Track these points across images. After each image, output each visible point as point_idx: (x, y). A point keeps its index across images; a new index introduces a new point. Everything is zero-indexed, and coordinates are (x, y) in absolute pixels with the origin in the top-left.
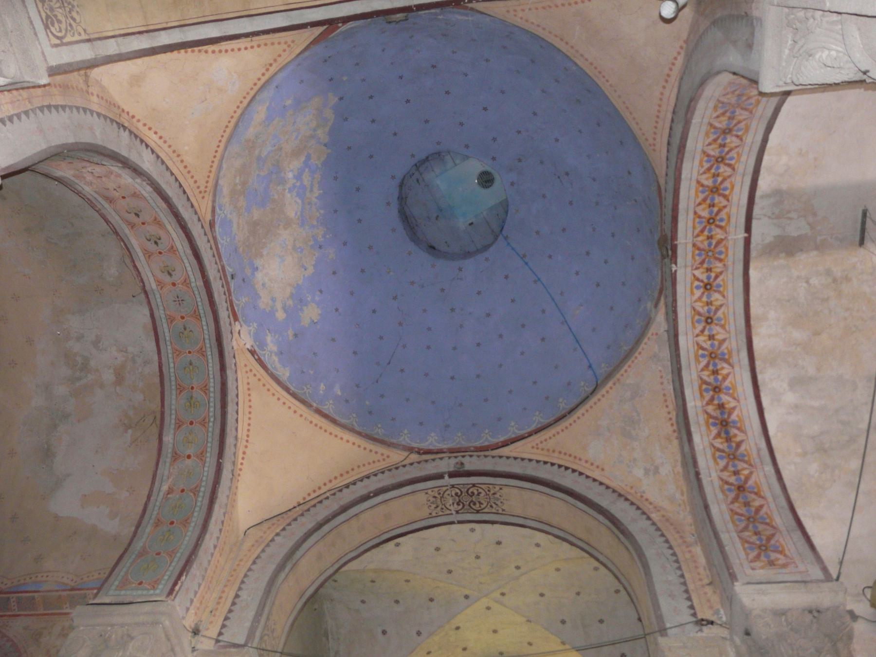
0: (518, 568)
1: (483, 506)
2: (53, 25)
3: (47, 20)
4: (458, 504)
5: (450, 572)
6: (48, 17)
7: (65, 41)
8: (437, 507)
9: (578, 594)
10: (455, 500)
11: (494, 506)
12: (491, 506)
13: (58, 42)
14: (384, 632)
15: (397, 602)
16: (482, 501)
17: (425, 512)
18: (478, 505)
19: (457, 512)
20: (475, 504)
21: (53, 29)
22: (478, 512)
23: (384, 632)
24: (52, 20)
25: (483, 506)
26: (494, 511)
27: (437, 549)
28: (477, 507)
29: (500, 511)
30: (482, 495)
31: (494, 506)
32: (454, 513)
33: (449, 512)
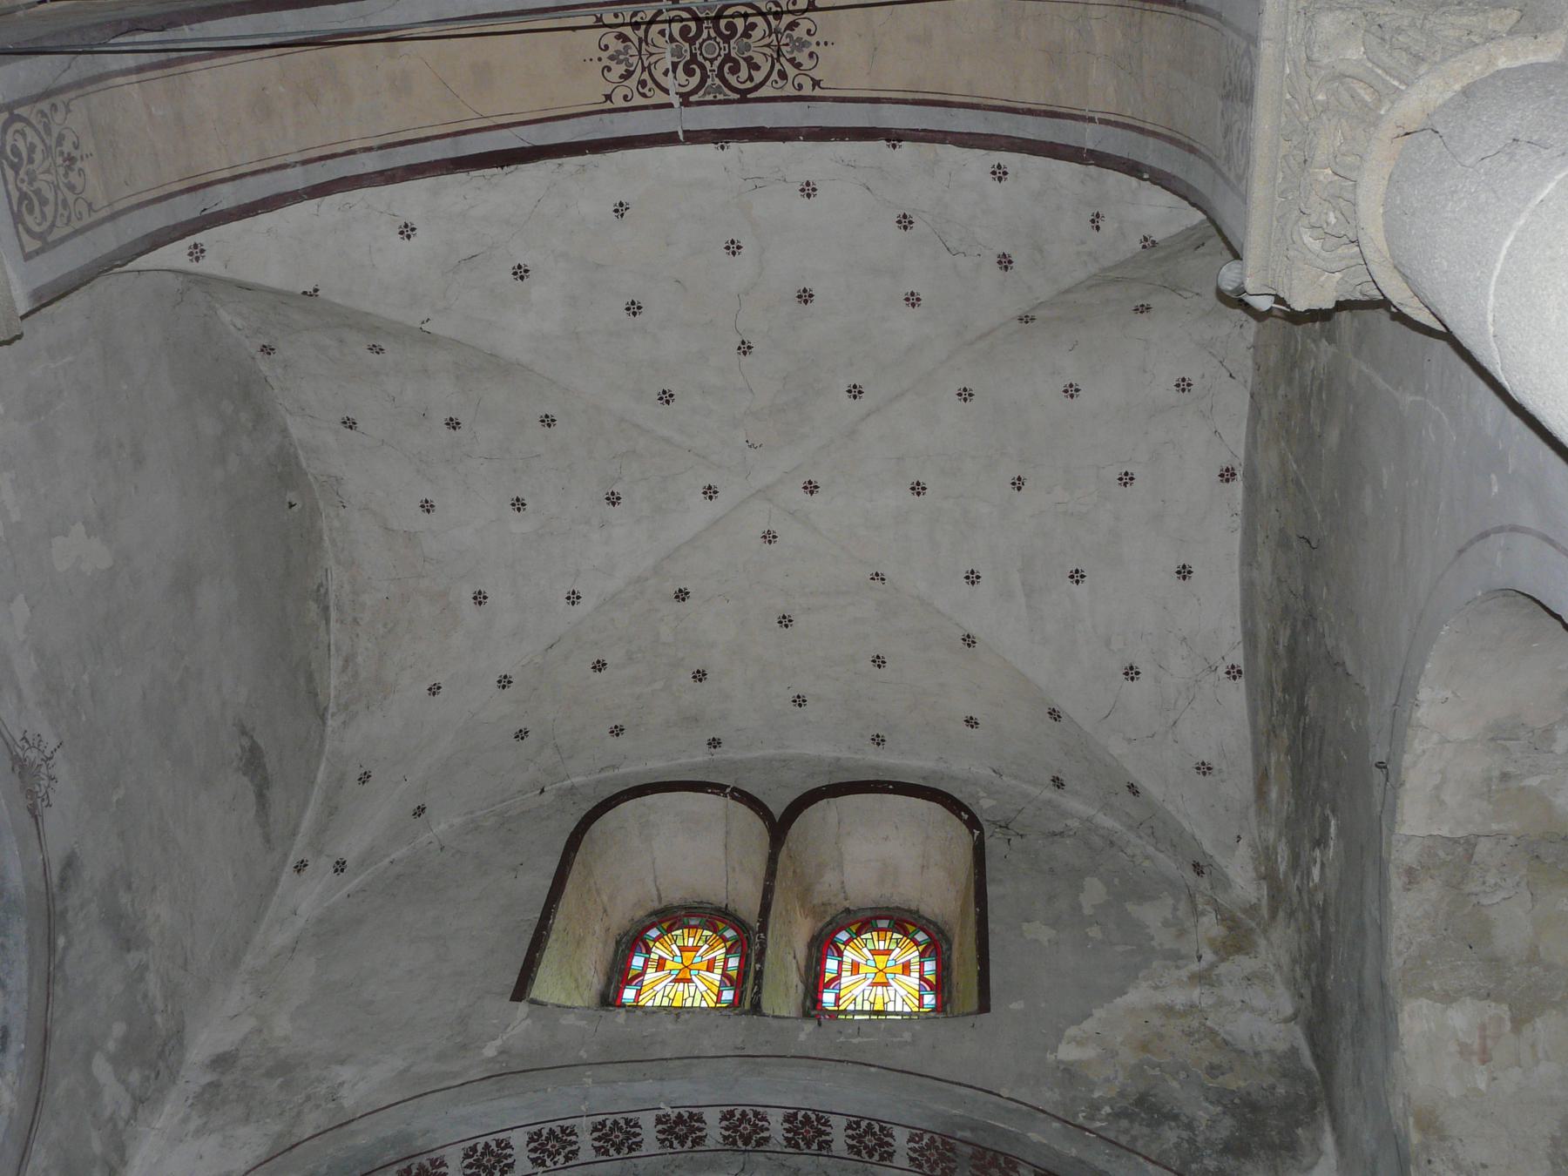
0: (855, 392)
1: (759, 76)
2: (31, 211)
3: (20, 203)
4: (689, 72)
5: (666, 397)
6: (23, 196)
7: (50, 239)
8: (627, 75)
9: (1018, 484)
10: (677, 53)
11: (791, 71)
12: (783, 75)
13: (37, 244)
14: (480, 598)
15: (519, 504)
16: (759, 59)
17: (591, 90)
18: (744, 74)
19: (685, 100)
20: (735, 70)
21: (29, 219)
22: (744, 97)
23: (480, 598)
24: (31, 200)
25: (759, 76)
26: (790, 91)
27: (634, 308)
28: (738, 80)
29: (807, 91)
30: (757, 34)
31: (791, 71)
32: (676, 101)
33: (659, 98)
